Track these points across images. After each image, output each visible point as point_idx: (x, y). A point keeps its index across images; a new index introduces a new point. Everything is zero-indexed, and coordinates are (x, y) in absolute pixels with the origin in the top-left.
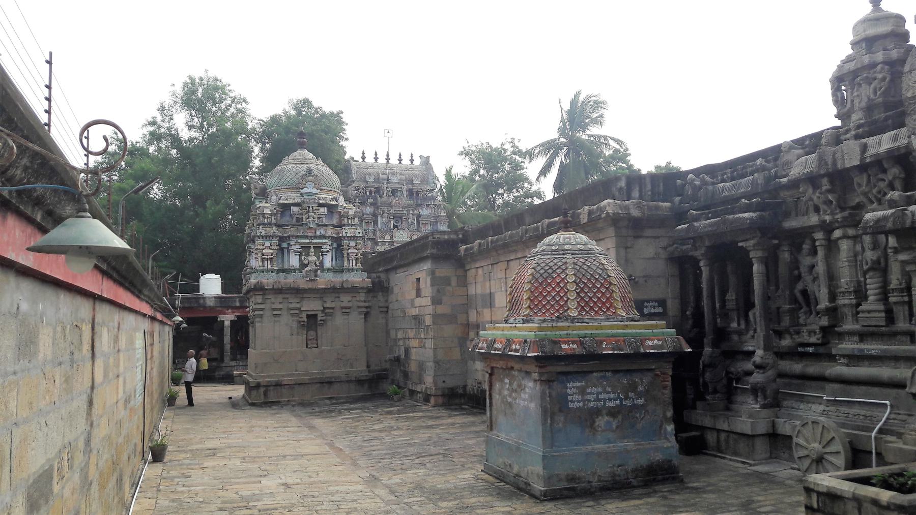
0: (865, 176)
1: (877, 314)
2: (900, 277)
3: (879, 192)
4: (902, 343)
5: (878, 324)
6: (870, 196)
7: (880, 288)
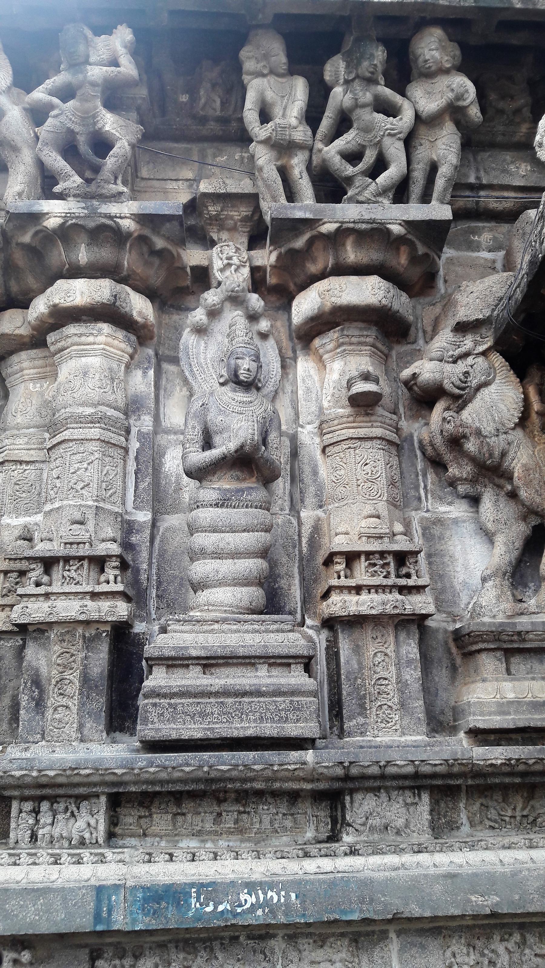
0: (300, 88)
1: (263, 677)
2: (382, 508)
3: (353, 157)
4: (386, 838)
5: (270, 730)
6: (298, 164)
7: (264, 553)
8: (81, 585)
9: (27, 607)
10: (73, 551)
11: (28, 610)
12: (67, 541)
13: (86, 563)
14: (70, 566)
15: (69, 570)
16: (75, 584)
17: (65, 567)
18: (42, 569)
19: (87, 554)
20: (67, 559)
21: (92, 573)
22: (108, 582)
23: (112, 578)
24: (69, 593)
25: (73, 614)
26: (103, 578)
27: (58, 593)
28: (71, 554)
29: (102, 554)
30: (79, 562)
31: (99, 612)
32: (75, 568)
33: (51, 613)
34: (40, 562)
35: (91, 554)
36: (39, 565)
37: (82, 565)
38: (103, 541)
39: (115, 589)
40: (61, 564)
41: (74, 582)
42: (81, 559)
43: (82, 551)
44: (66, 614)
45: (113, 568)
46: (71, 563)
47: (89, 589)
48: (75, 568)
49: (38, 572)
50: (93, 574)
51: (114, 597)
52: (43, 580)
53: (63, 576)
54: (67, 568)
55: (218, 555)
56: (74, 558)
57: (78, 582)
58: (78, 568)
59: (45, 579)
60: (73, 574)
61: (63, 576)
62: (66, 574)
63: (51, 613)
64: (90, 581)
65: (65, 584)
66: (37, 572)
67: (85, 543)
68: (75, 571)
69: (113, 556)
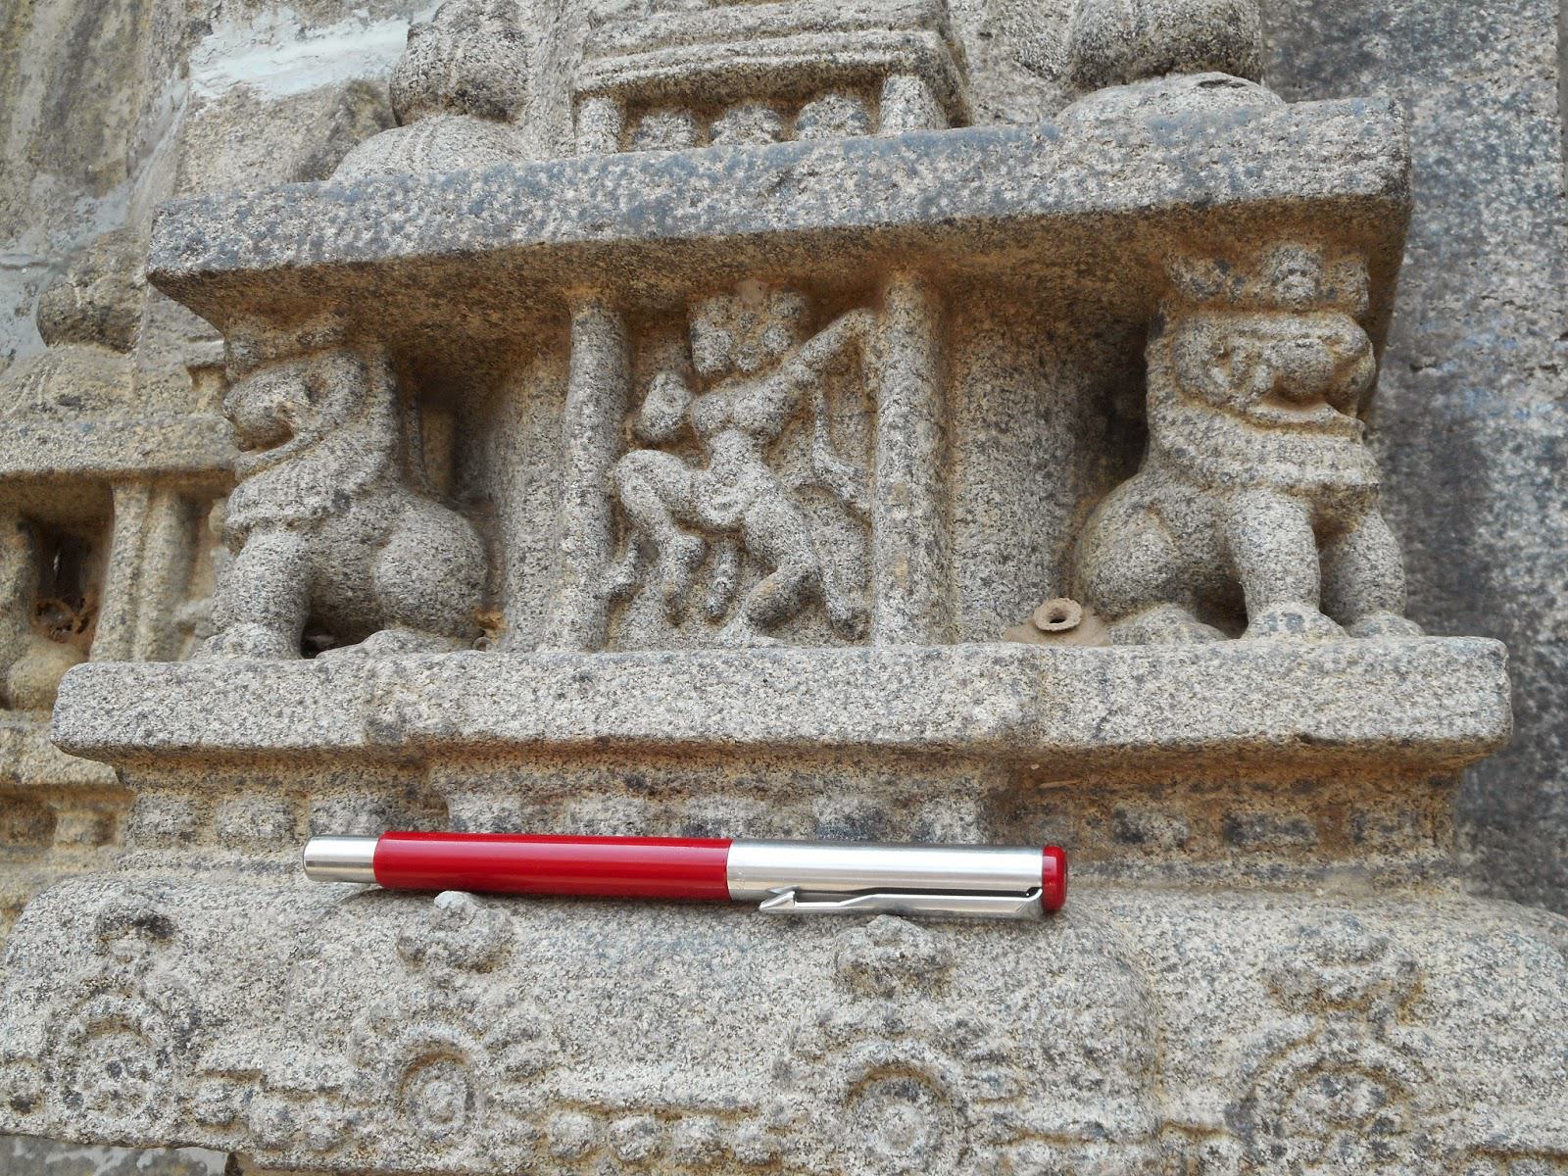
8: (853, 630)
9: (157, 928)
10: (721, 183)
11: (167, 965)
12: (634, 69)
13: (896, 344)
14: (699, 383)
15: (686, 441)
16: (774, 620)
17: (631, 402)
18: (375, 430)
19: (903, 202)
20: (656, 300)
21: (974, 476)
22: (1223, 604)
23: (1275, 538)
24: (682, 752)
25: (747, 1083)
26: (1132, 538)
27: (535, 749)
28: (690, 218)
29: (1125, 195)
30: (808, 327)
31: (1147, 1070)
32: (754, 402)
33: (431, 1058)
34: (347, 342)
35: (964, 205)
36: (338, 375)
37: (847, 370)
38: (1093, 71)
39: (1356, 713)
40: (590, 354)
41: (761, 590)
42: (830, 280)
43: (835, 177)
44: (647, 1079)
45: (1284, 393)
46: (710, 343)
47: (971, 692)
48: (754, 402)
49: (324, 461)
50: (1003, 497)
51: (1340, 832)
52: (386, 569)
53: (619, 523)
54: (661, 405)
55: (144, 534)
56: (723, 268)
57: (808, 597)
58: (797, 414)
59: (418, 547)
60: (741, 488)
61: (619, 523)
62: (650, 480)
63: (431, 1058)
64: (969, 577)
65: (644, 618)
66: (320, 468)
67: (867, 83)
68: (769, 443)
69: (1271, 220)
